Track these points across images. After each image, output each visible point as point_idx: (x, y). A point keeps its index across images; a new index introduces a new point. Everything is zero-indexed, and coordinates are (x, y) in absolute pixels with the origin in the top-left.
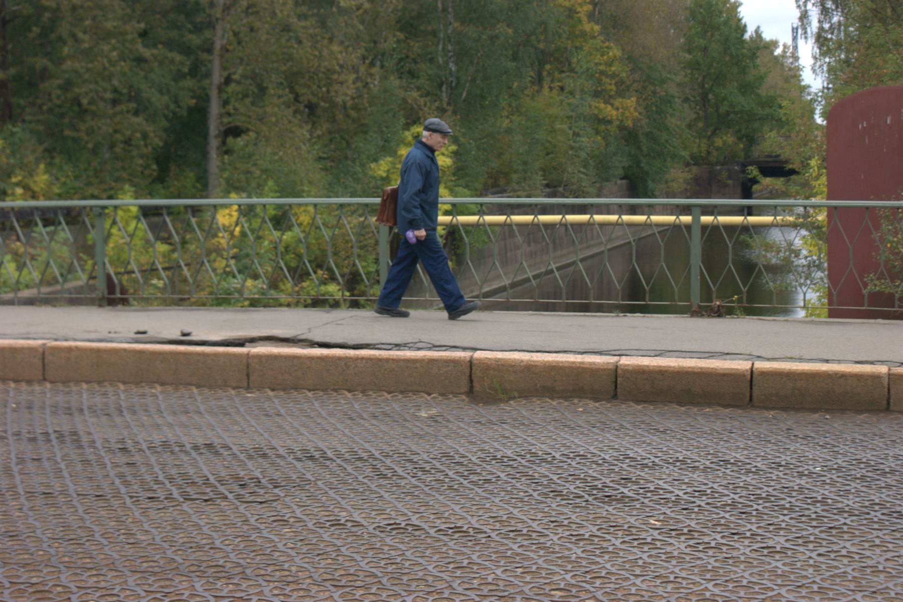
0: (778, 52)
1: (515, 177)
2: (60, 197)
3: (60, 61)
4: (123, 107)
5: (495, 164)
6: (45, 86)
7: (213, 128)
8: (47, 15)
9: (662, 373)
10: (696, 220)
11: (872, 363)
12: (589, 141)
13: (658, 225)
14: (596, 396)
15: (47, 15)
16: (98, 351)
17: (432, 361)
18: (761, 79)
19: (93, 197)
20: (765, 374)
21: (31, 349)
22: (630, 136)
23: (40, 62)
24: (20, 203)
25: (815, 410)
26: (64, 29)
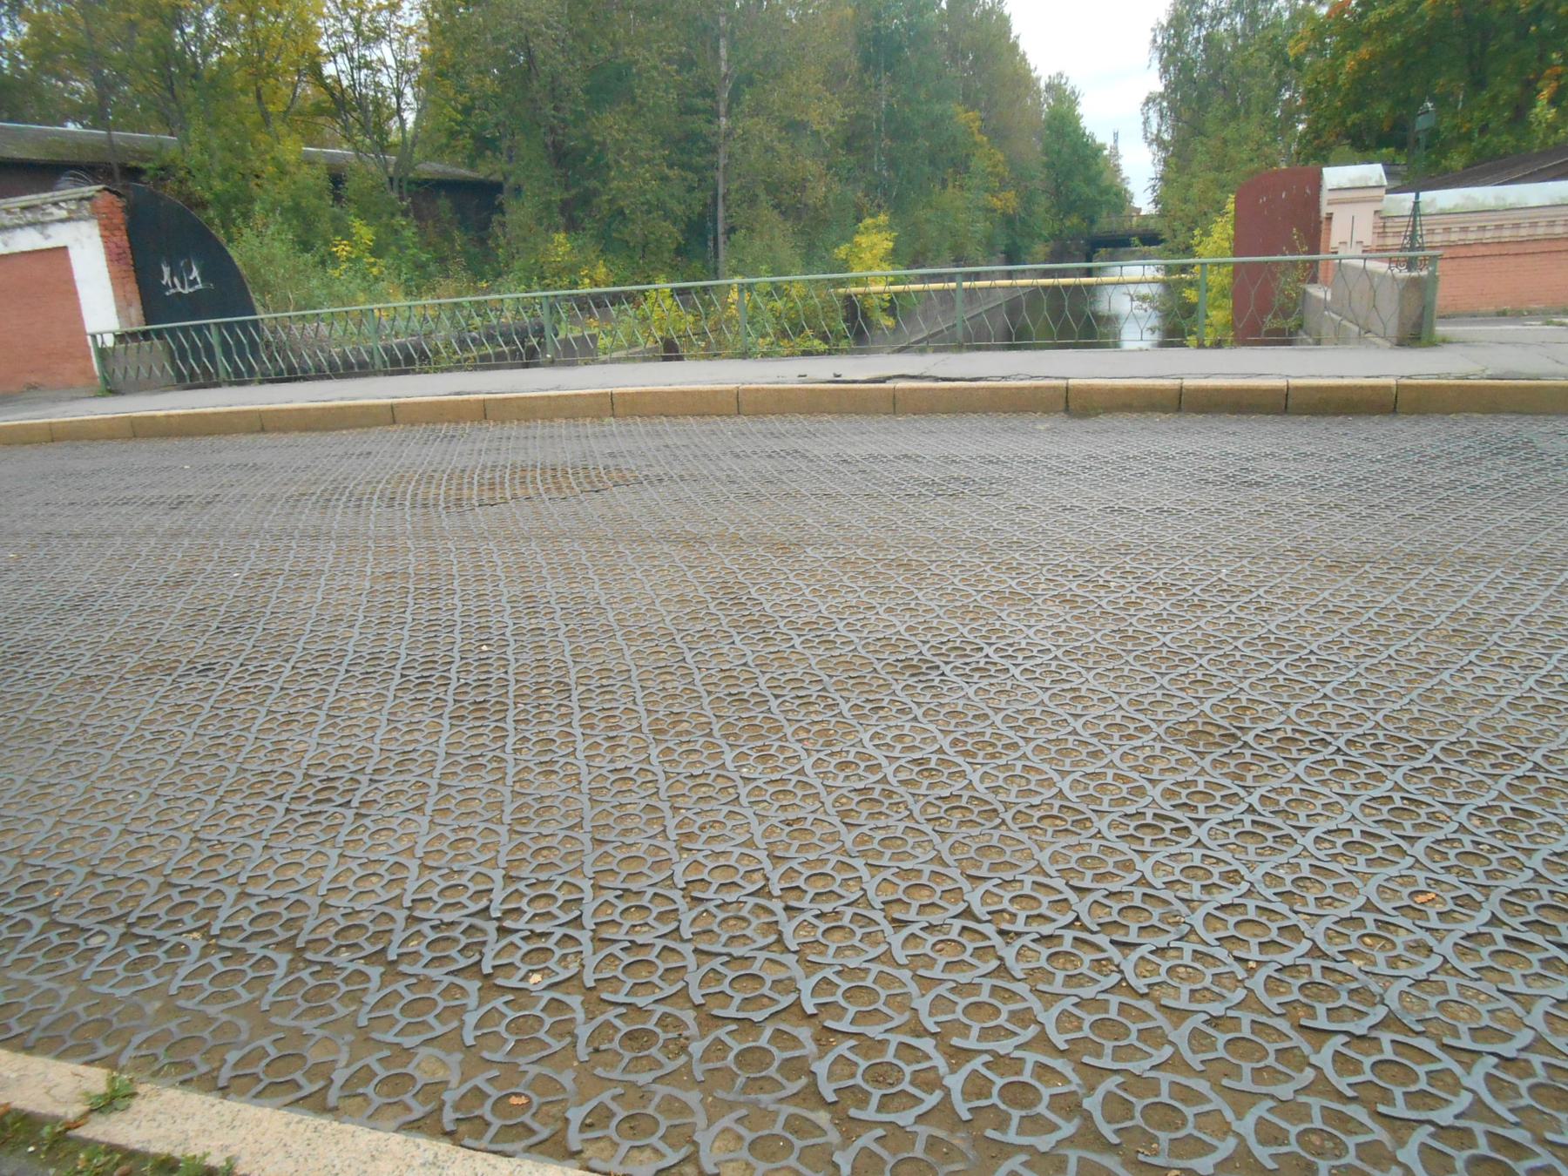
0: (1106, 153)
1: (930, 255)
2: (615, 284)
3: (605, 183)
4: (655, 215)
5: (918, 246)
6: (596, 201)
7: (721, 228)
8: (597, 147)
10: (959, 285)
12: (982, 226)
13: (1023, 287)
14: (1164, 409)
15: (597, 147)
16: (778, 391)
17: (1037, 388)
18: (1100, 173)
19: (637, 283)
20: (1297, 388)
21: (728, 391)
22: (1009, 221)
23: (593, 183)
24: (588, 290)
25: (1336, 414)
26: (610, 157)
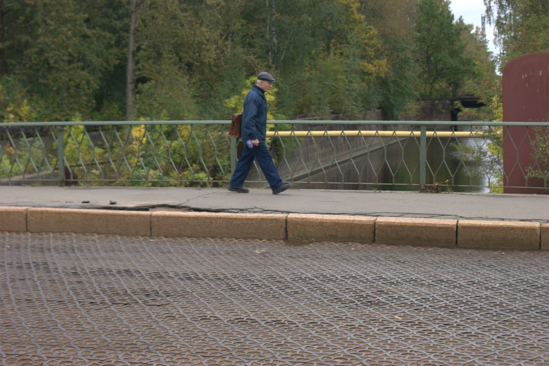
0: (473, 31)
1: (313, 107)
2: (37, 119)
3: (37, 37)
4: (75, 65)
5: (301, 100)
6: (27, 52)
7: (130, 78)
8: (29, 9)
9: (403, 227)
10: (423, 134)
11: (530, 221)
12: (358, 86)
13: (400, 137)
14: (362, 241)
15: (29, 9)
16: (60, 213)
17: (263, 219)
18: (463, 48)
19: (57, 120)
20: (465, 227)
21: (19, 212)
22: (383, 83)
23: (25, 38)
24: (12, 124)
25: (495, 249)
26: (39, 17)
